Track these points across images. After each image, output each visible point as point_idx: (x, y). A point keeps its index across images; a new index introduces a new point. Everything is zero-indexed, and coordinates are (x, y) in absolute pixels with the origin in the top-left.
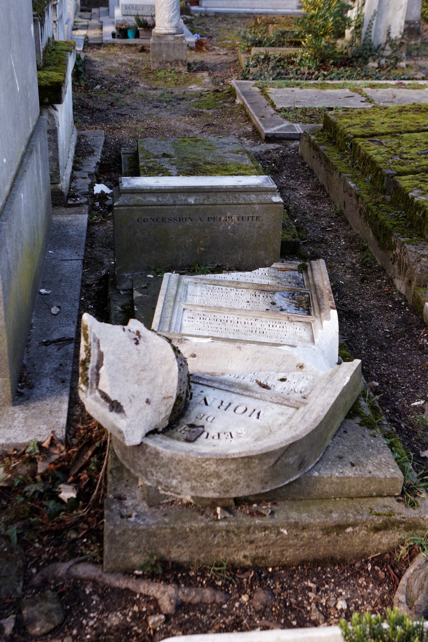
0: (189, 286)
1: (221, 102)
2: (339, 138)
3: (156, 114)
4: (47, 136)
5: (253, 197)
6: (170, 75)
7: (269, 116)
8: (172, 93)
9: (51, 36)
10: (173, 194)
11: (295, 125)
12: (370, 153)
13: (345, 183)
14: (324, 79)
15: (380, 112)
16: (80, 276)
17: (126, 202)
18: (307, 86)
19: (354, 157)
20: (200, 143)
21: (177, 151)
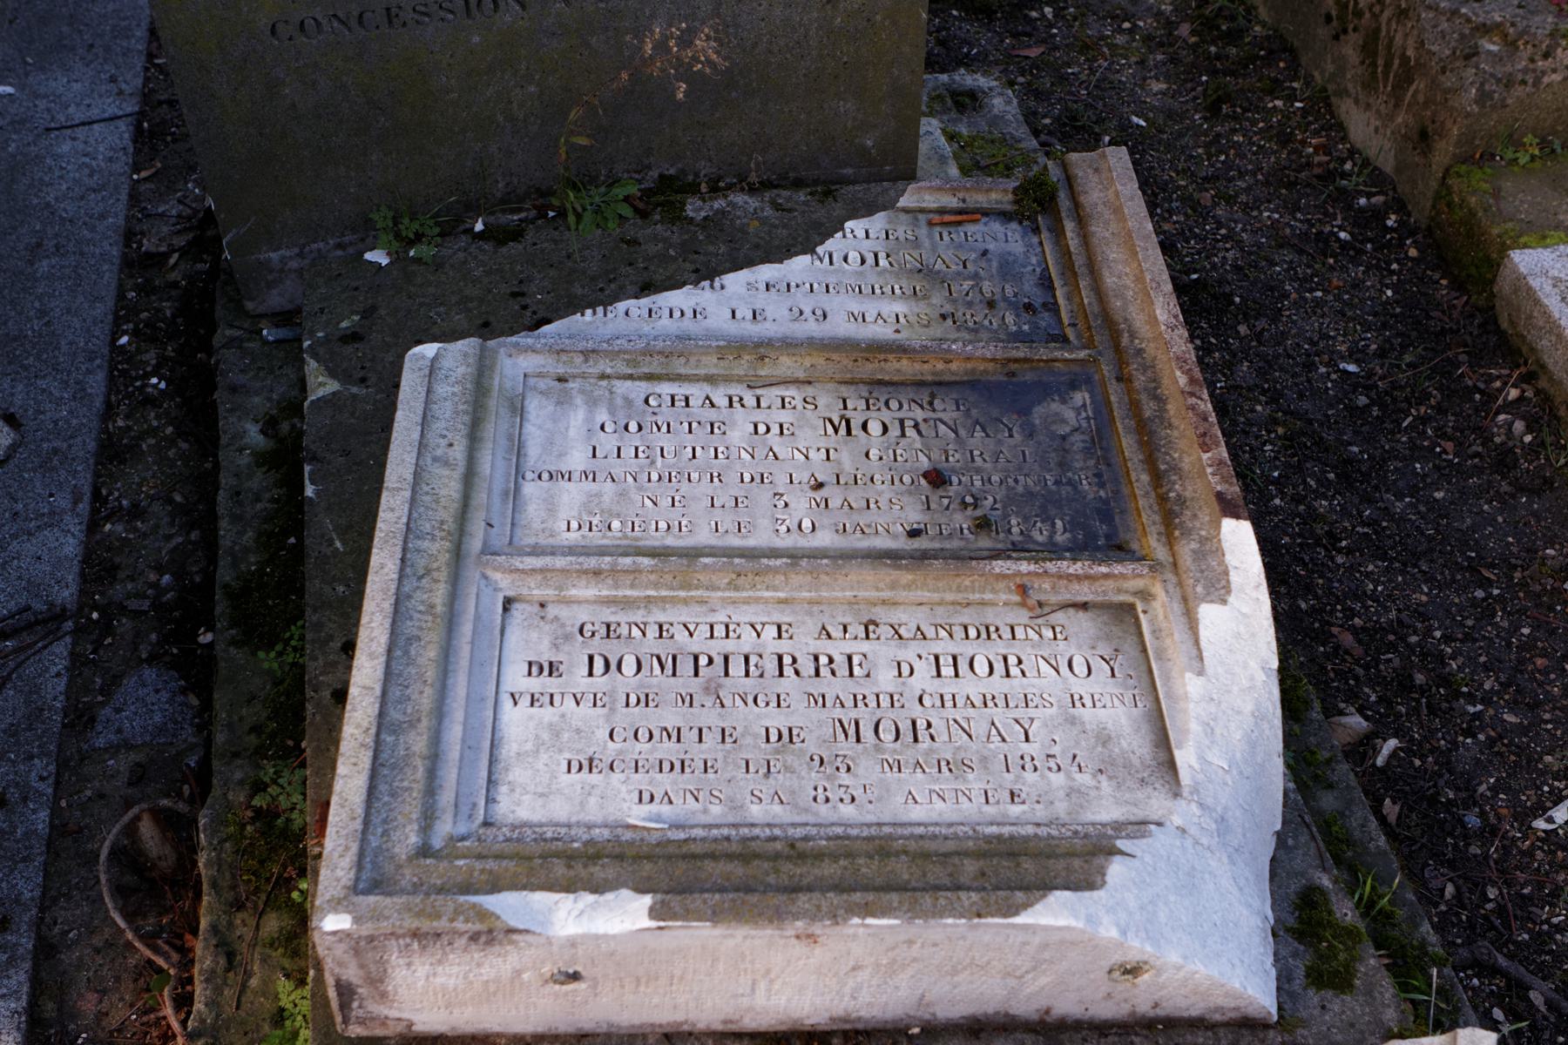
0: (533, 405)
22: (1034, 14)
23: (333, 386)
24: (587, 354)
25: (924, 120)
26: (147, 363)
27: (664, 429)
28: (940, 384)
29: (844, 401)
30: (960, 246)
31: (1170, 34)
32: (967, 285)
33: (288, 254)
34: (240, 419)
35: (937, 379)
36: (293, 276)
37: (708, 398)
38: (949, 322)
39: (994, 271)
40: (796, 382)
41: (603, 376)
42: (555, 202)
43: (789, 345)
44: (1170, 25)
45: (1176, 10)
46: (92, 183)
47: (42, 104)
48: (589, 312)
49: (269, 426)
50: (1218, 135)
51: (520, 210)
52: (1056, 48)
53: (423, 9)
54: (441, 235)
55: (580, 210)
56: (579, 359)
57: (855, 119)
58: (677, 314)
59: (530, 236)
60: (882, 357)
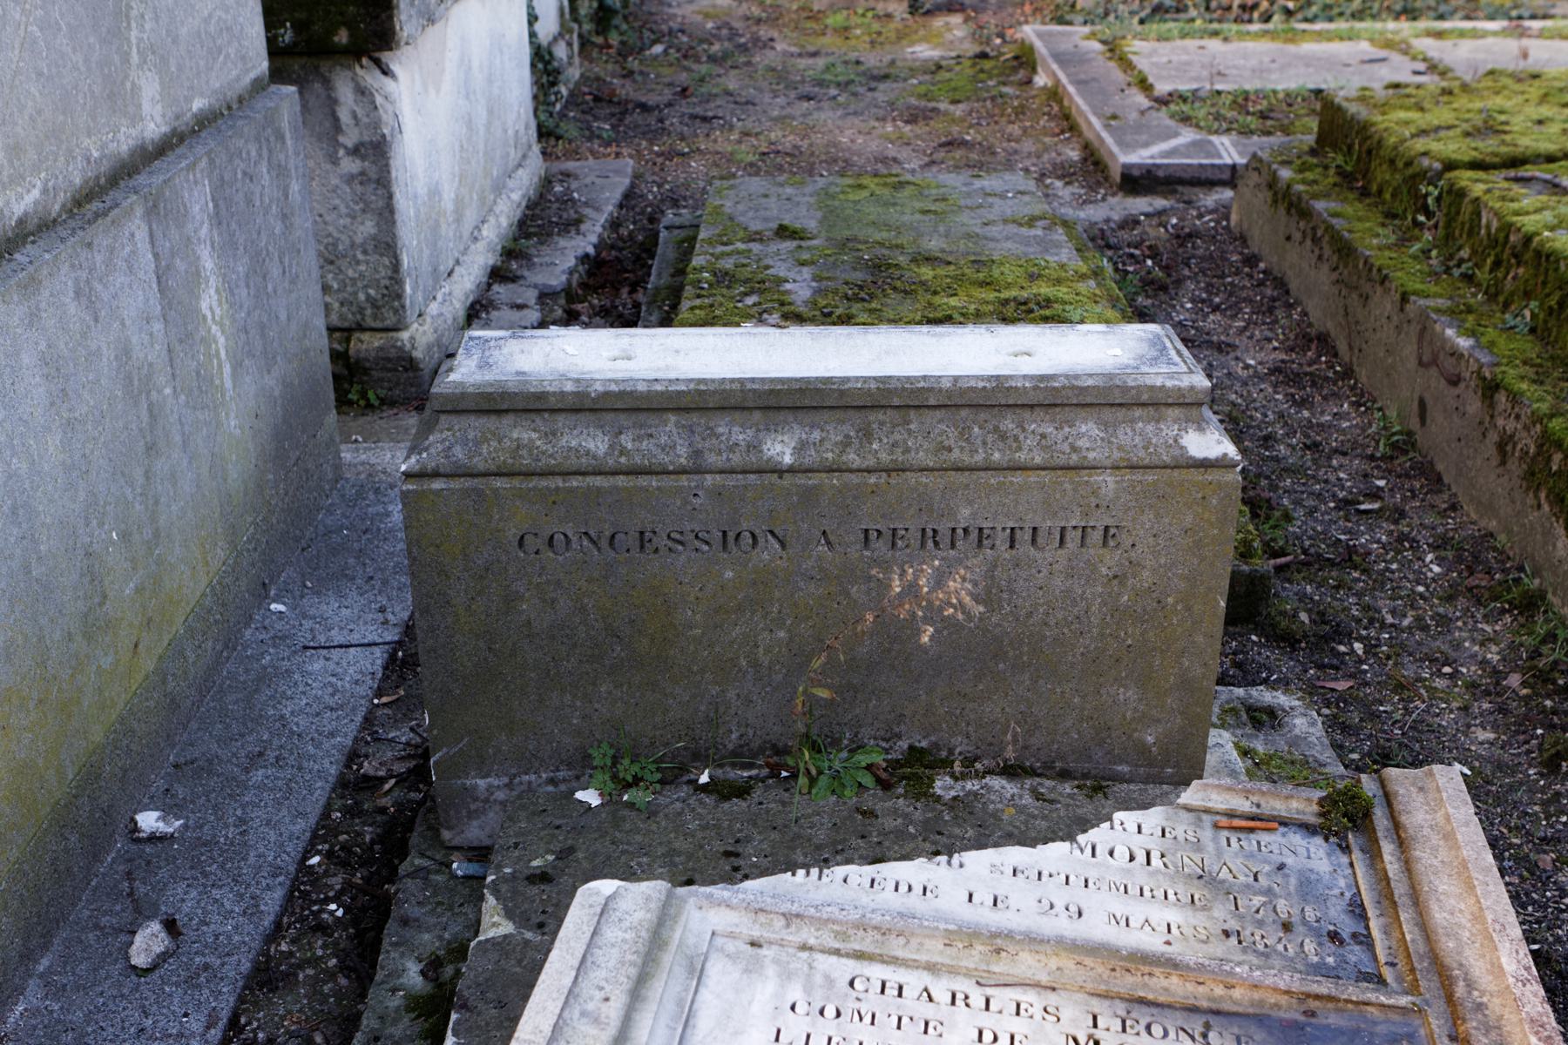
1: (991, 83)
2: (1381, 174)
3: (804, 115)
5: (1088, 433)
6: (859, 21)
7: (1134, 115)
8: (858, 62)
10: (695, 417)
11: (1214, 139)
12: (1529, 223)
13: (1424, 330)
14: (1287, 21)
15: (1517, 87)
16: (349, 730)
17: (459, 453)
18: (1242, 36)
19: (1449, 237)
20: (908, 191)
21: (830, 216)
22: (1342, 648)
23: (507, 928)
24: (789, 918)
25: (1213, 732)
26: (331, 887)
27: (868, 1019)
28: (1217, 1013)
29: (1095, 1018)
30: (1251, 856)
31: (1498, 683)
32: (1257, 900)
33: (496, 783)
34: (402, 955)
35: (1214, 1006)
36: (497, 808)
37: (926, 990)
38: (1233, 940)
39: (1292, 888)
40: (1036, 985)
41: (804, 947)
42: (791, 762)
43: (1033, 941)
44: (1497, 675)
45: (1504, 659)
46: (331, 702)
47: (307, 624)
48: (801, 872)
49: (432, 967)
50: (1558, 794)
51: (750, 766)
52: (1366, 684)
53: (678, 536)
54: (662, 782)
55: (814, 772)
56: (779, 923)
57: (1135, 710)
58: (903, 888)
59: (757, 794)
60: (1147, 969)
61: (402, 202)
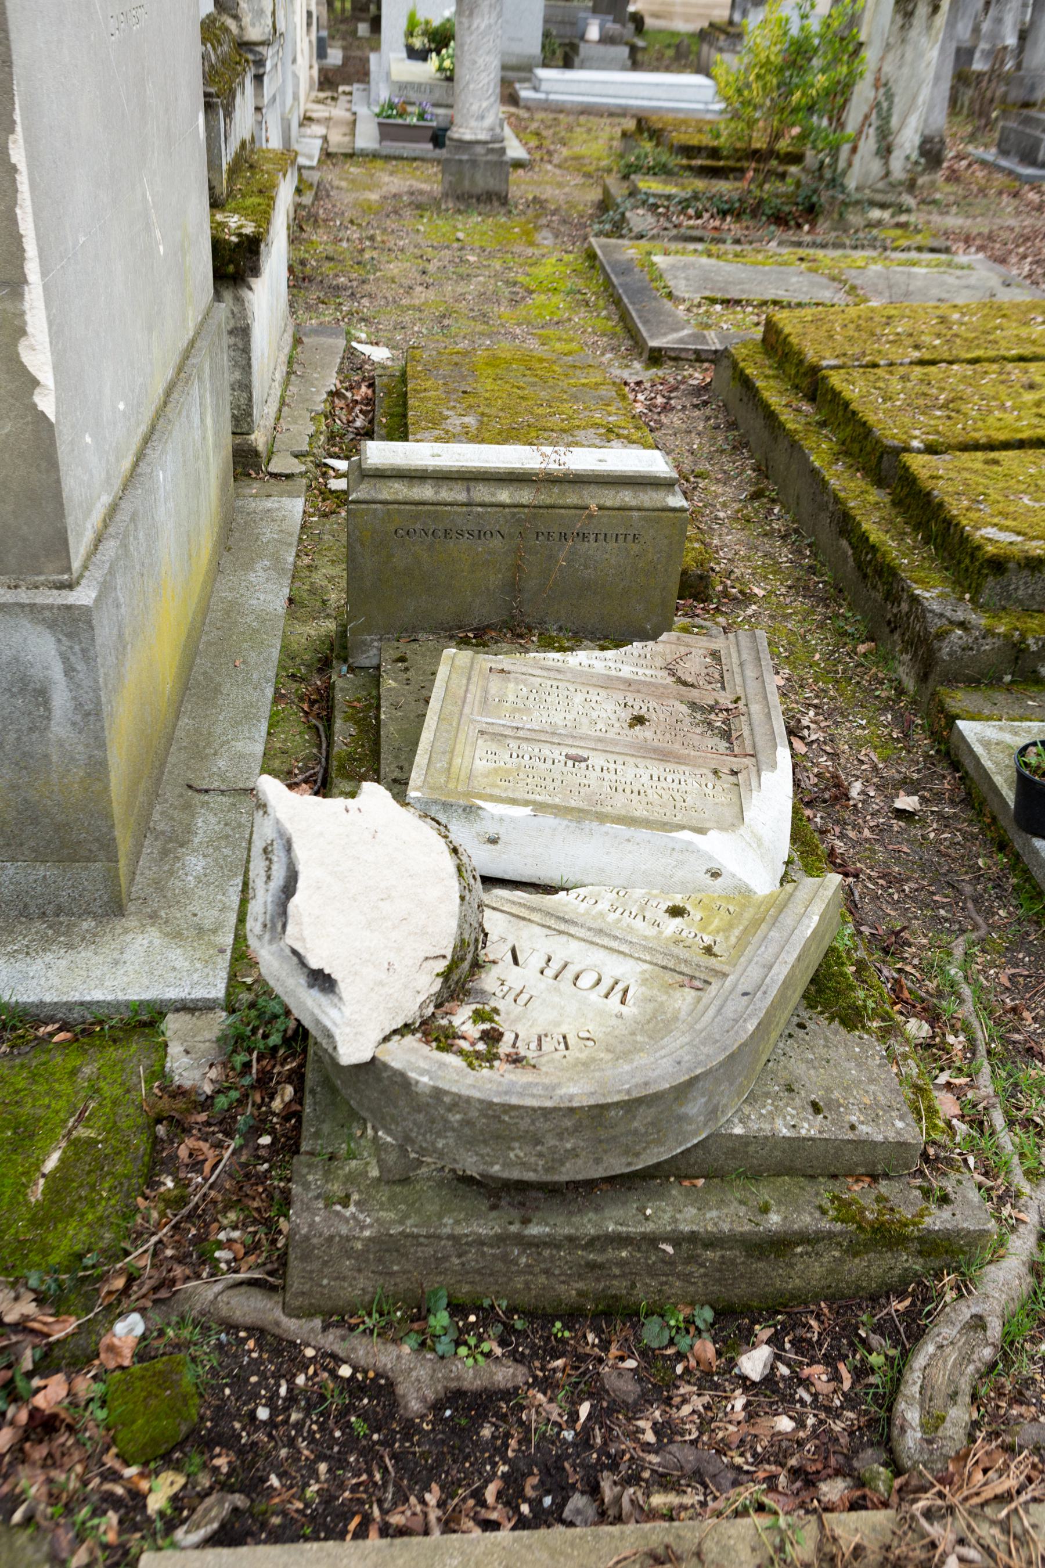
4: (227, 340)
9: (248, 137)
61: (255, 363)
